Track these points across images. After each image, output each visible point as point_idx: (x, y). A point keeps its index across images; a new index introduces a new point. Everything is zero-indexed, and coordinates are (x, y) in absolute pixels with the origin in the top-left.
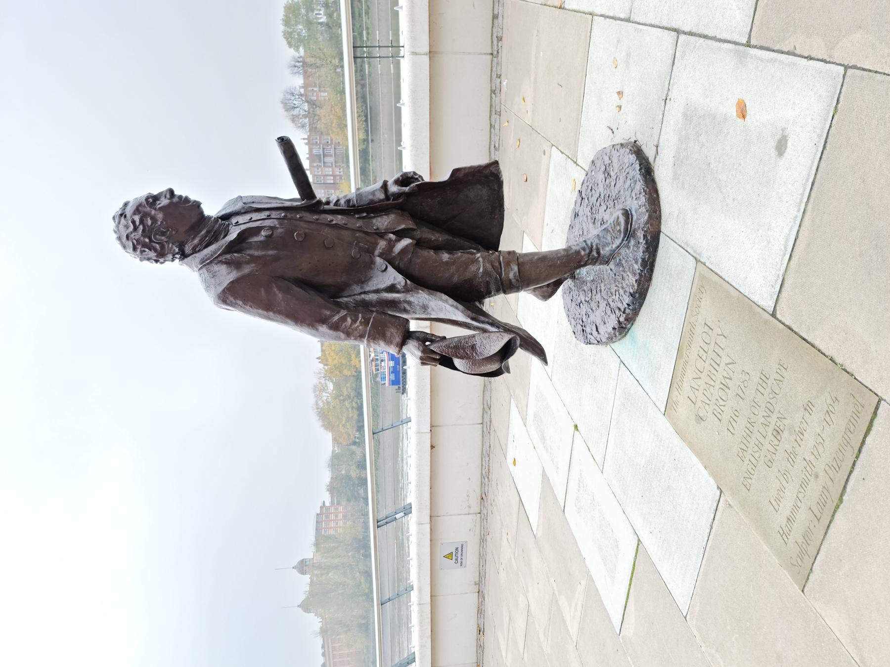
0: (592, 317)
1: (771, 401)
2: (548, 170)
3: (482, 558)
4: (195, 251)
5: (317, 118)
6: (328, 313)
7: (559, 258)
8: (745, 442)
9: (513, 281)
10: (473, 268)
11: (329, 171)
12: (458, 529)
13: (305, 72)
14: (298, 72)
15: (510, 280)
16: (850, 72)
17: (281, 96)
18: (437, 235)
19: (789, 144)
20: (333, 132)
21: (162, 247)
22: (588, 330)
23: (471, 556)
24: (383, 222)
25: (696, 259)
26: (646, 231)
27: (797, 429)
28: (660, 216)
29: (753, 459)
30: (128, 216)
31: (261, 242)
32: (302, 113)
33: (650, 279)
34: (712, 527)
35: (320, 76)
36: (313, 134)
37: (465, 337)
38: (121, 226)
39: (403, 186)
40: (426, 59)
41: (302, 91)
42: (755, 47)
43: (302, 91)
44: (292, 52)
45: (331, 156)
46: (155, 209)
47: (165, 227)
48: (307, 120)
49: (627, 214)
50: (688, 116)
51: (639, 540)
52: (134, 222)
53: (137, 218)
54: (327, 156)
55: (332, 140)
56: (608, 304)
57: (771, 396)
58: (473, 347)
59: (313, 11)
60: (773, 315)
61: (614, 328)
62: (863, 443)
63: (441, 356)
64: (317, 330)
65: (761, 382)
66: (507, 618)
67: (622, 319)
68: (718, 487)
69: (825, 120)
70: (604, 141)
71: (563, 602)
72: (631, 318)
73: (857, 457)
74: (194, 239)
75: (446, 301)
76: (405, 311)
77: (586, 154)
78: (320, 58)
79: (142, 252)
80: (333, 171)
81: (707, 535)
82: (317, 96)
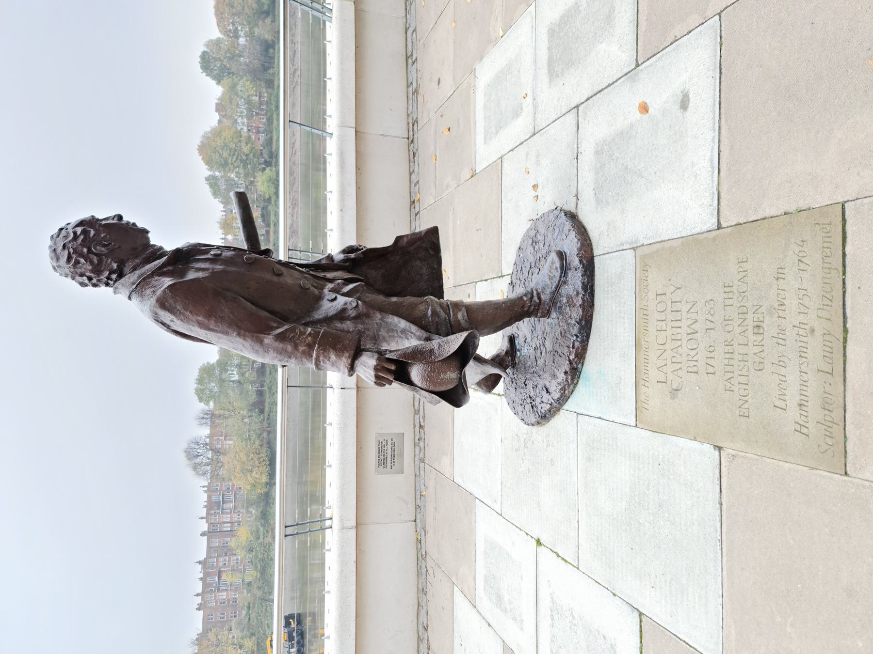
1: (742, 304)
5: (220, 464)
7: (504, 303)
9: (462, 322)
11: (227, 518)
13: (213, 423)
14: (206, 423)
17: (185, 446)
19: (691, 96)
21: (100, 262)
27: (776, 306)
28: (591, 244)
32: (206, 461)
33: (592, 304)
34: (721, 504)
36: (214, 481)
41: (208, 440)
43: (208, 440)
44: (202, 406)
45: (230, 502)
47: (105, 250)
48: (209, 468)
49: (561, 255)
51: (641, 614)
54: (226, 502)
55: (233, 485)
57: (740, 299)
59: (227, 371)
61: (566, 373)
62: (844, 255)
64: (261, 342)
65: (726, 296)
67: (572, 357)
72: (581, 355)
73: (844, 274)
78: (229, 410)
80: (231, 518)
81: (718, 519)
82: (222, 444)
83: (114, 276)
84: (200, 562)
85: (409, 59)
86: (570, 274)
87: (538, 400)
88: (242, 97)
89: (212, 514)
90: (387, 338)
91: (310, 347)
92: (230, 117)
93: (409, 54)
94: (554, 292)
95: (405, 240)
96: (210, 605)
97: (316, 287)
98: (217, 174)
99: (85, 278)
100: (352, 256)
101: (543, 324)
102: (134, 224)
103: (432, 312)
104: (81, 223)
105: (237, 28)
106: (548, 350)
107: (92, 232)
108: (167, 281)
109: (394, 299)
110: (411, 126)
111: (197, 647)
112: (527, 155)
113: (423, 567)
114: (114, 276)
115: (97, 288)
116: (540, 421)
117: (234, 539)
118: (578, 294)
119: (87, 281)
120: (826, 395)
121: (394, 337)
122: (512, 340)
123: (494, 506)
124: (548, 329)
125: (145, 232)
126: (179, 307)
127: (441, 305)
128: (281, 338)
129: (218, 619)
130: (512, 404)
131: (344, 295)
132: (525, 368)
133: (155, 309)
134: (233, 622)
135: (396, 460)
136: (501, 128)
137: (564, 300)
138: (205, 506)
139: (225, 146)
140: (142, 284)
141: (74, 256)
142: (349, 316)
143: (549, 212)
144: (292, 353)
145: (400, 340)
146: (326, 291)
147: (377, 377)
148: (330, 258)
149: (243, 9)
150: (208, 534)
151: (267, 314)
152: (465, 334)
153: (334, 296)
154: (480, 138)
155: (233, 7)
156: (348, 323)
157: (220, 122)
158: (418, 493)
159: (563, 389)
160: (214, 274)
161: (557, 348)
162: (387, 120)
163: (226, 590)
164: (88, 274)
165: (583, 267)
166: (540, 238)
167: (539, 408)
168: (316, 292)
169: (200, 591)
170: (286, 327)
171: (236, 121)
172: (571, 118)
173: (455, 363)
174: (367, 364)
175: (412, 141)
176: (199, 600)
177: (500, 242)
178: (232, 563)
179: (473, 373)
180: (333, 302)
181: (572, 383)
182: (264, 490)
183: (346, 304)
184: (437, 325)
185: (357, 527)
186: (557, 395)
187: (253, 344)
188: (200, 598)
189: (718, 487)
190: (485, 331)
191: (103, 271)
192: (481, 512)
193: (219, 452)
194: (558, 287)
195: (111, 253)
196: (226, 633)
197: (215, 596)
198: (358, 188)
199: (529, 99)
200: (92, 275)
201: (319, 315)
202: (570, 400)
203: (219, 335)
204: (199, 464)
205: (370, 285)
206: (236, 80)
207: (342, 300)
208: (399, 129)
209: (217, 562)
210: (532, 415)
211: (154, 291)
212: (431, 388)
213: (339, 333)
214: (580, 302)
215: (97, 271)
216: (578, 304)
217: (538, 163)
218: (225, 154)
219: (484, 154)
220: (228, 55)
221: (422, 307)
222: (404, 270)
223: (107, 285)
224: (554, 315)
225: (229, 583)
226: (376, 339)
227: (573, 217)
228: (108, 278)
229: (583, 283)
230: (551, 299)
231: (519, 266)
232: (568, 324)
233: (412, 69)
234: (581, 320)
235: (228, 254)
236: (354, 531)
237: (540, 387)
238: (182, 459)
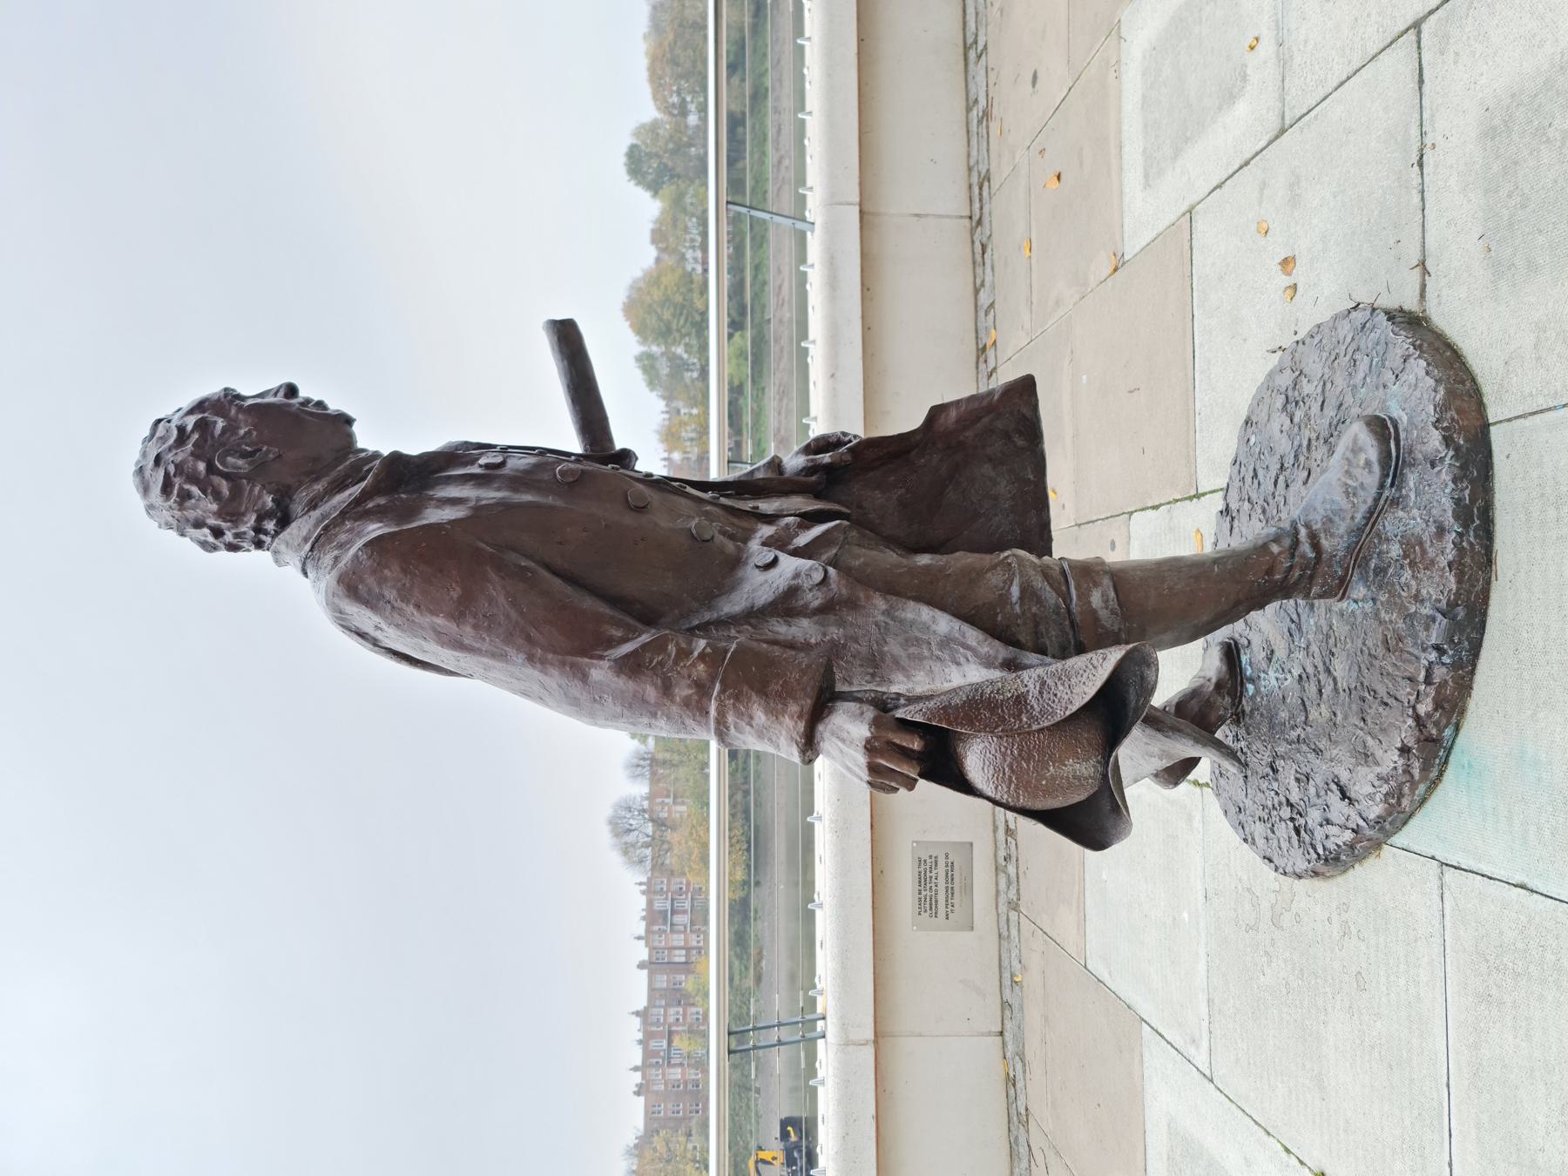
5: (665, 846)
7: (1215, 561)
9: (1103, 614)
11: (678, 940)
13: (654, 774)
14: (642, 775)
15: (1094, 612)
20: (691, 870)
21: (236, 492)
35: (676, 779)
41: (646, 804)
43: (646, 804)
45: (685, 912)
47: (254, 465)
48: (648, 852)
49: (1382, 428)
55: (688, 884)
61: (1404, 750)
64: (584, 678)
72: (1453, 702)
78: (679, 752)
79: (185, 496)
80: (686, 941)
82: (670, 811)
83: (270, 526)
84: (637, 1013)
85: (971, 50)
86: (1412, 479)
87: (1314, 816)
88: (693, 215)
90: (904, 662)
91: (702, 689)
92: (675, 251)
93: (970, 40)
94: (1360, 530)
95: (953, 414)
96: (655, 1088)
97: (732, 537)
98: (655, 349)
99: (206, 531)
100: (826, 458)
101: (1320, 615)
102: (320, 404)
103: (1023, 591)
104: (200, 406)
105: (684, 101)
106: (1342, 684)
107: (220, 423)
108: (375, 529)
109: (924, 560)
110: (976, 190)
111: (635, 1160)
112: (1263, 186)
113: (1022, 1140)
114: (270, 526)
115: (240, 554)
116: (1320, 866)
117: (691, 978)
118: (1441, 531)
119: (211, 539)
121: (921, 658)
122: (1231, 653)
123: (1191, 1051)
124: (1341, 629)
125: (349, 421)
126: (390, 594)
127: (1045, 573)
128: (631, 666)
129: (670, 1114)
130: (1237, 813)
131: (797, 553)
132: (1272, 727)
133: (336, 600)
134: (694, 1122)
135: (956, 901)
136: (1187, 140)
137: (1395, 550)
139: (667, 300)
140: (323, 539)
141: (177, 481)
142: (806, 606)
143: (1336, 318)
144: (657, 705)
145: (936, 667)
146: (754, 545)
147: (873, 769)
148: (776, 465)
149: (694, 66)
150: (652, 965)
151: (604, 609)
152: (1115, 655)
153: (770, 557)
154: (1132, 178)
155: (677, 64)
156: (805, 622)
157: (658, 260)
158: (1007, 975)
159: (1395, 795)
160: (480, 513)
161: (1373, 679)
162: (926, 184)
163: (681, 1065)
164: (212, 521)
165: (1456, 457)
166: (1307, 388)
167: (1319, 833)
168: (730, 546)
169: (639, 1062)
170: (645, 638)
171: (683, 257)
172: (1399, 61)
173: (1090, 735)
174: (849, 728)
175: (979, 222)
176: (637, 1077)
177: (1190, 414)
178: (689, 1020)
179: (1138, 754)
180: (771, 572)
181: (1423, 778)
182: (740, 894)
183: (797, 575)
184: (1037, 625)
185: (876, 1042)
186: (1375, 810)
187: (564, 681)
188: (639, 1074)
190: (1167, 637)
191: (243, 514)
192: (1156, 1059)
193: (663, 824)
194: (1373, 515)
195: (259, 471)
196: (682, 1139)
198: (867, 329)
199: (1266, 49)
200: (224, 525)
201: (733, 604)
202: (1413, 822)
203: (485, 660)
204: (633, 845)
205: (865, 525)
206: (683, 186)
207: (789, 565)
208: (951, 199)
209: (665, 1015)
210: (1297, 853)
211: (336, 559)
212: (1023, 802)
213: (777, 651)
214: (1450, 553)
215: (231, 513)
216: (1443, 562)
217: (1294, 201)
218: (667, 315)
219: (1144, 212)
220: (671, 146)
221: (995, 579)
222: (956, 486)
223: (259, 545)
224: (1358, 591)
225: (684, 1052)
226: (876, 664)
227: (1413, 322)
228: (258, 530)
229: (1458, 502)
230: (1349, 549)
231: (1246, 467)
232: (1409, 617)
233: (978, 71)
234: (1452, 605)
235: (517, 463)
236: (870, 1050)
237: (1318, 779)
238: (605, 835)
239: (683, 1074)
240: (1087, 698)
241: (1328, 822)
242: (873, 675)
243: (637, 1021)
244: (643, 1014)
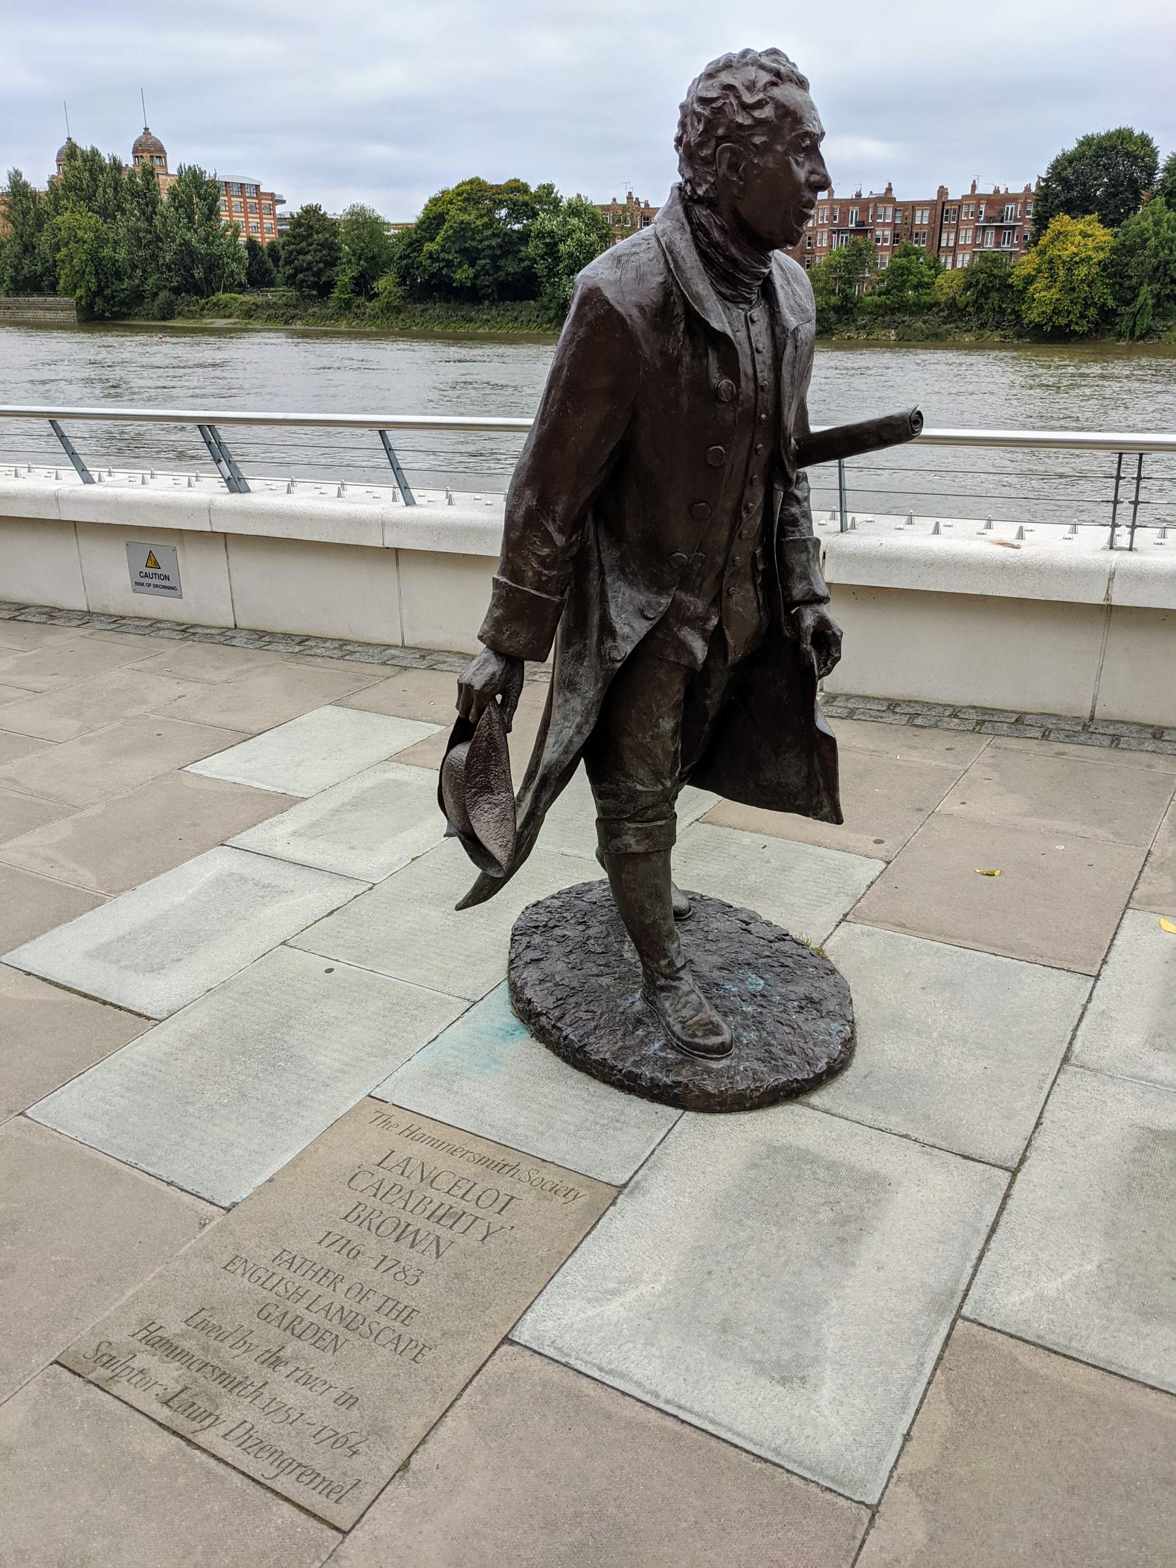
0: (557, 950)
2: (845, 849)
3: (153, 626)
4: (697, 231)
6: (560, 509)
8: (305, 1268)
10: (642, 773)
11: (966, 237)
12: (207, 589)
15: (620, 836)
16: (866, 1514)
18: (716, 697)
22: (537, 939)
23: (153, 604)
24: (744, 601)
25: (625, 1186)
26: (686, 1086)
29: (275, 1280)
30: (776, 92)
31: (707, 378)
34: (169, 1184)
37: (507, 771)
38: (752, 73)
39: (814, 635)
40: (1098, 598)
42: (952, 1328)
45: (998, 244)
46: (786, 153)
50: (873, 1185)
52: (760, 105)
53: (767, 112)
54: (998, 235)
56: (574, 991)
57: (374, 1326)
58: (488, 789)
60: (507, 1340)
63: (479, 721)
65: (400, 1307)
66: (35, 686)
68: (234, 1205)
69: (800, 1464)
70: (871, 997)
71: (62, 829)
72: (542, 1035)
74: (721, 229)
75: (579, 731)
76: (567, 643)
77: (853, 952)
80: (964, 247)
84: (889, 190)
89: (978, 206)
120: (152, 1382)
138: (997, 191)
165: (666, 1085)
189: (189, 1189)
197: (823, 226)
239: (822, 249)
240: (476, 831)
241: (527, 947)
242: (564, 682)
243: (880, 190)
244: (887, 198)
